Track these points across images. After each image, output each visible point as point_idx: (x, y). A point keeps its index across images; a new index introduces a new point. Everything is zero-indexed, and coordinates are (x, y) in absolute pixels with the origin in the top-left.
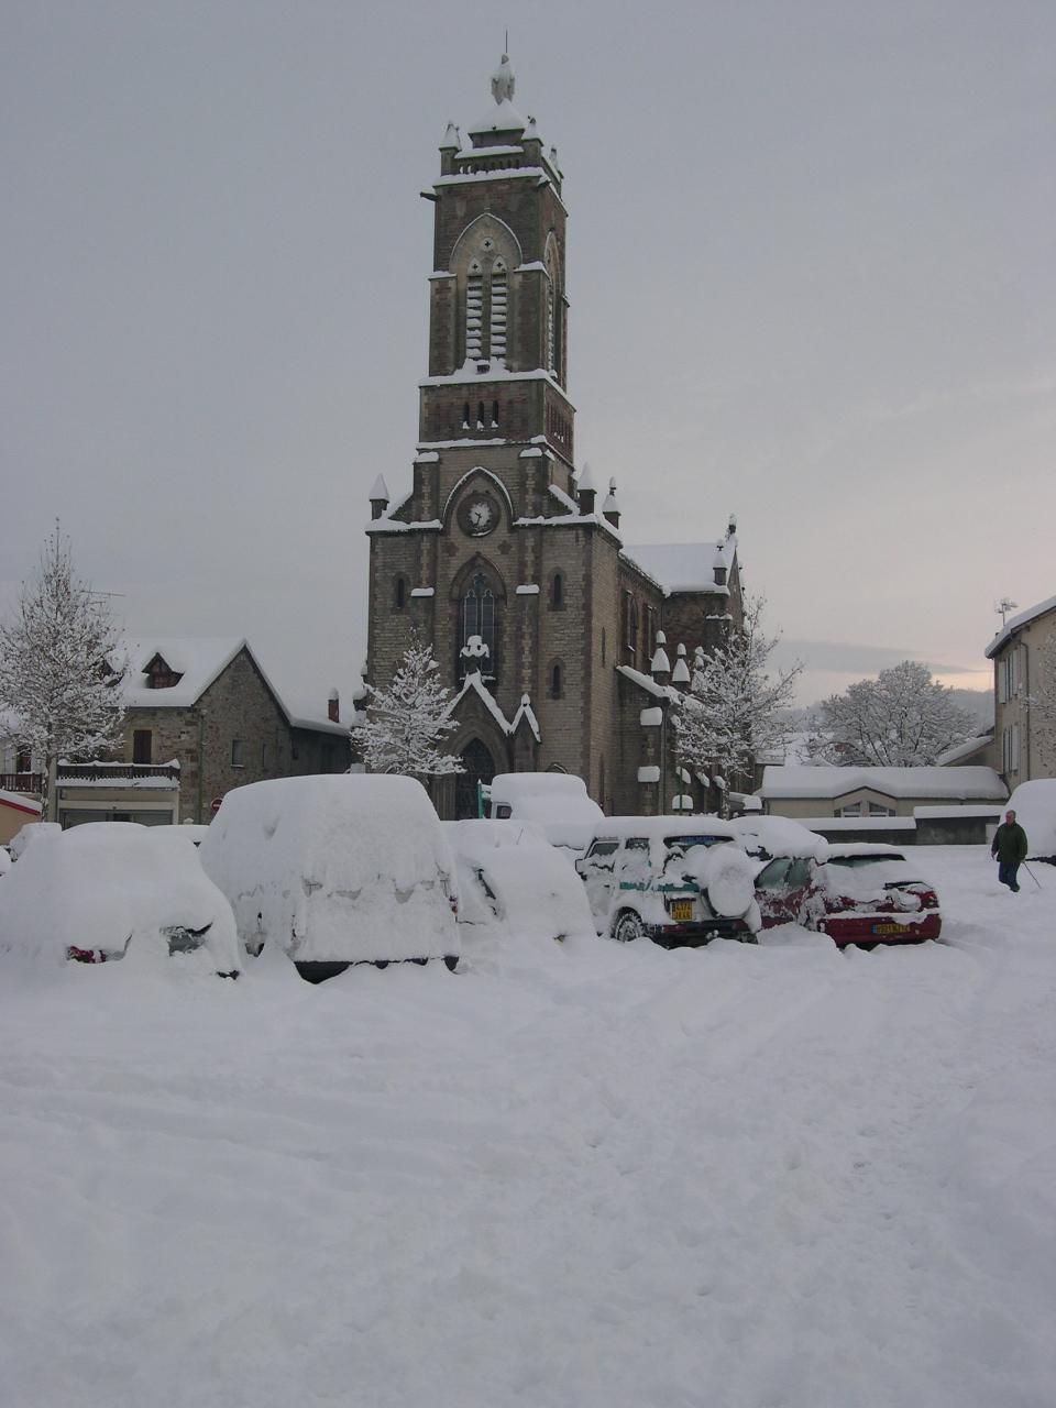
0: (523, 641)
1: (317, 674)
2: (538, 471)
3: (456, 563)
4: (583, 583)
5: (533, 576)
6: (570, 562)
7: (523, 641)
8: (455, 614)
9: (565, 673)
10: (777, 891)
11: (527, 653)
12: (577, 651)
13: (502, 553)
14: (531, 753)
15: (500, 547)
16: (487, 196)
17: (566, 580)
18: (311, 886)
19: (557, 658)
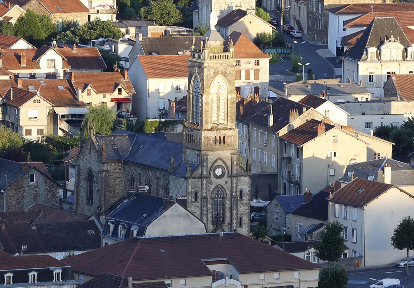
0: (234, 211)
1: (331, 15)
2: (237, 159)
3: (212, 187)
4: (248, 193)
5: (235, 191)
6: (245, 186)
7: (234, 211)
8: (212, 203)
9: (243, 220)
10: (83, 41)
11: (235, 215)
12: (247, 213)
13: (226, 184)
14: (208, 188)
15: (225, 182)
16: (220, 67)
17: (244, 192)
18: (183, 231)
19: (241, 215)
